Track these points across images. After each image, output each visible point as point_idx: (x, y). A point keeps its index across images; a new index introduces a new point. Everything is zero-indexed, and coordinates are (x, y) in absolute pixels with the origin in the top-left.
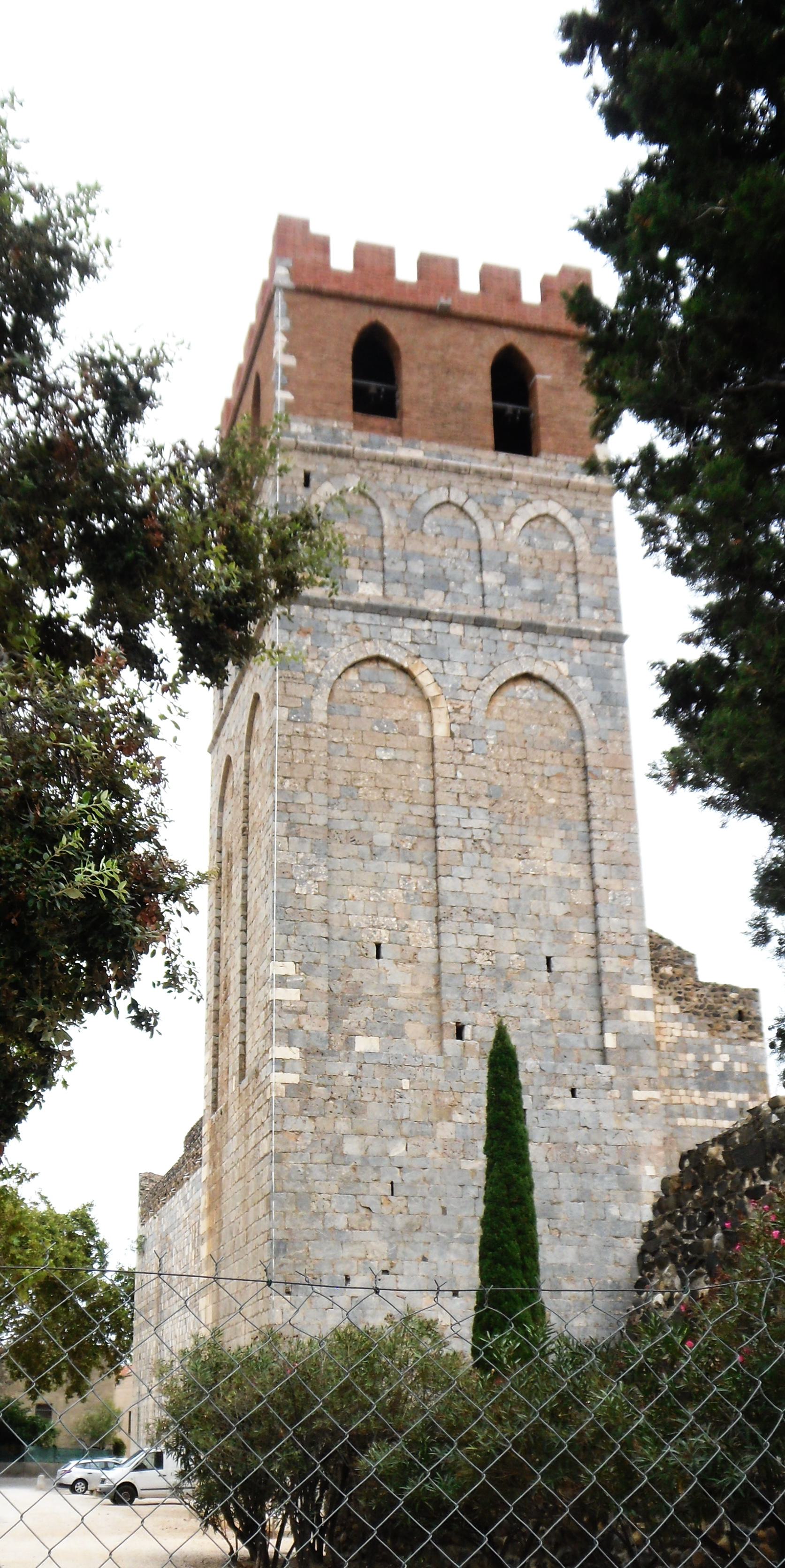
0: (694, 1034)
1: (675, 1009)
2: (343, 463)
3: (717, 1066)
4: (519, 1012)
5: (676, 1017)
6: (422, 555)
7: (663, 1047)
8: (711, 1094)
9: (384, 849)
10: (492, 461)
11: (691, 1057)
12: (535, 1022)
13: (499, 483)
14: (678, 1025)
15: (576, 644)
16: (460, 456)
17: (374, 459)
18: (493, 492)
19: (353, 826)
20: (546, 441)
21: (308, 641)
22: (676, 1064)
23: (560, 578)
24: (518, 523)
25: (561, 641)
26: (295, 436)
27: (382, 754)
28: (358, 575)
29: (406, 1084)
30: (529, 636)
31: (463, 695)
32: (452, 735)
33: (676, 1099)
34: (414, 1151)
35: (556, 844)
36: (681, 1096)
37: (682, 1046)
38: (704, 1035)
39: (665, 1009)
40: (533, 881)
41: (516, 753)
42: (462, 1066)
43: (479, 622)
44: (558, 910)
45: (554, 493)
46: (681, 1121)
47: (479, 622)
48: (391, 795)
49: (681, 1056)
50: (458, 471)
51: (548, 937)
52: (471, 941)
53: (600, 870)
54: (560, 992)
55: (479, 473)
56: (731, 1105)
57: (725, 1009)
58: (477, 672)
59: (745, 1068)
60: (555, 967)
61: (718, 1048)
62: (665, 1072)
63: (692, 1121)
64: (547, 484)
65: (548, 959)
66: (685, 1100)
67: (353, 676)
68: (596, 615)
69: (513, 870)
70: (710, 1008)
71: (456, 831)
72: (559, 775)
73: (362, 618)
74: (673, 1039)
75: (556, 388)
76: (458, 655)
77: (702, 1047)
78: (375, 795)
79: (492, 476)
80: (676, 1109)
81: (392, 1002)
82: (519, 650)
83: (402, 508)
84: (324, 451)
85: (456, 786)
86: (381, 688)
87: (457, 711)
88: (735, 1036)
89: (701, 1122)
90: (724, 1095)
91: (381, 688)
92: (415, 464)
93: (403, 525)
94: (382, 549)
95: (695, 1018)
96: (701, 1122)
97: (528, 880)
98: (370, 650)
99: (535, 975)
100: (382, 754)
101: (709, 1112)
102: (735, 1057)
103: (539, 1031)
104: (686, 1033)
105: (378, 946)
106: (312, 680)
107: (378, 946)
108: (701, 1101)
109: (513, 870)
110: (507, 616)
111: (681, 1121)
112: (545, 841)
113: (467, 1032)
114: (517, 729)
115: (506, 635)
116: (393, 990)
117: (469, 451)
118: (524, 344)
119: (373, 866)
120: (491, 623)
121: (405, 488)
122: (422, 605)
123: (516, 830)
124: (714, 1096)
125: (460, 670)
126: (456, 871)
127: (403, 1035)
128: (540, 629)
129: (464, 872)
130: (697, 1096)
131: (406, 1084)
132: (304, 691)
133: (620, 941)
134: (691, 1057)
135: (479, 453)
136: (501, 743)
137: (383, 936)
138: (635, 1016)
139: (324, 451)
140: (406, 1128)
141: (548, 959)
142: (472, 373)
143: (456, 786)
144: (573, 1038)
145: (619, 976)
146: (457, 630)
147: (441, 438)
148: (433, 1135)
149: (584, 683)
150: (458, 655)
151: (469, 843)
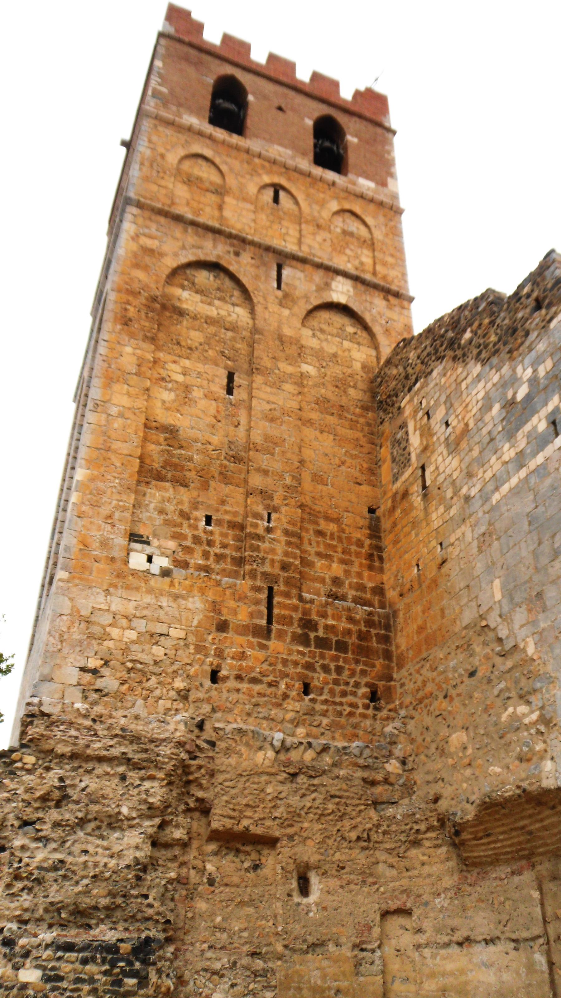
3: (522, 392)
5: (479, 378)
8: (520, 435)
22: (485, 431)
56: (542, 426)
57: (520, 315)
59: (549, 364)
62: (475, 453)
74: (480, 405)
88: (535, 334)
89: (514, 481)
102: (535, 364)
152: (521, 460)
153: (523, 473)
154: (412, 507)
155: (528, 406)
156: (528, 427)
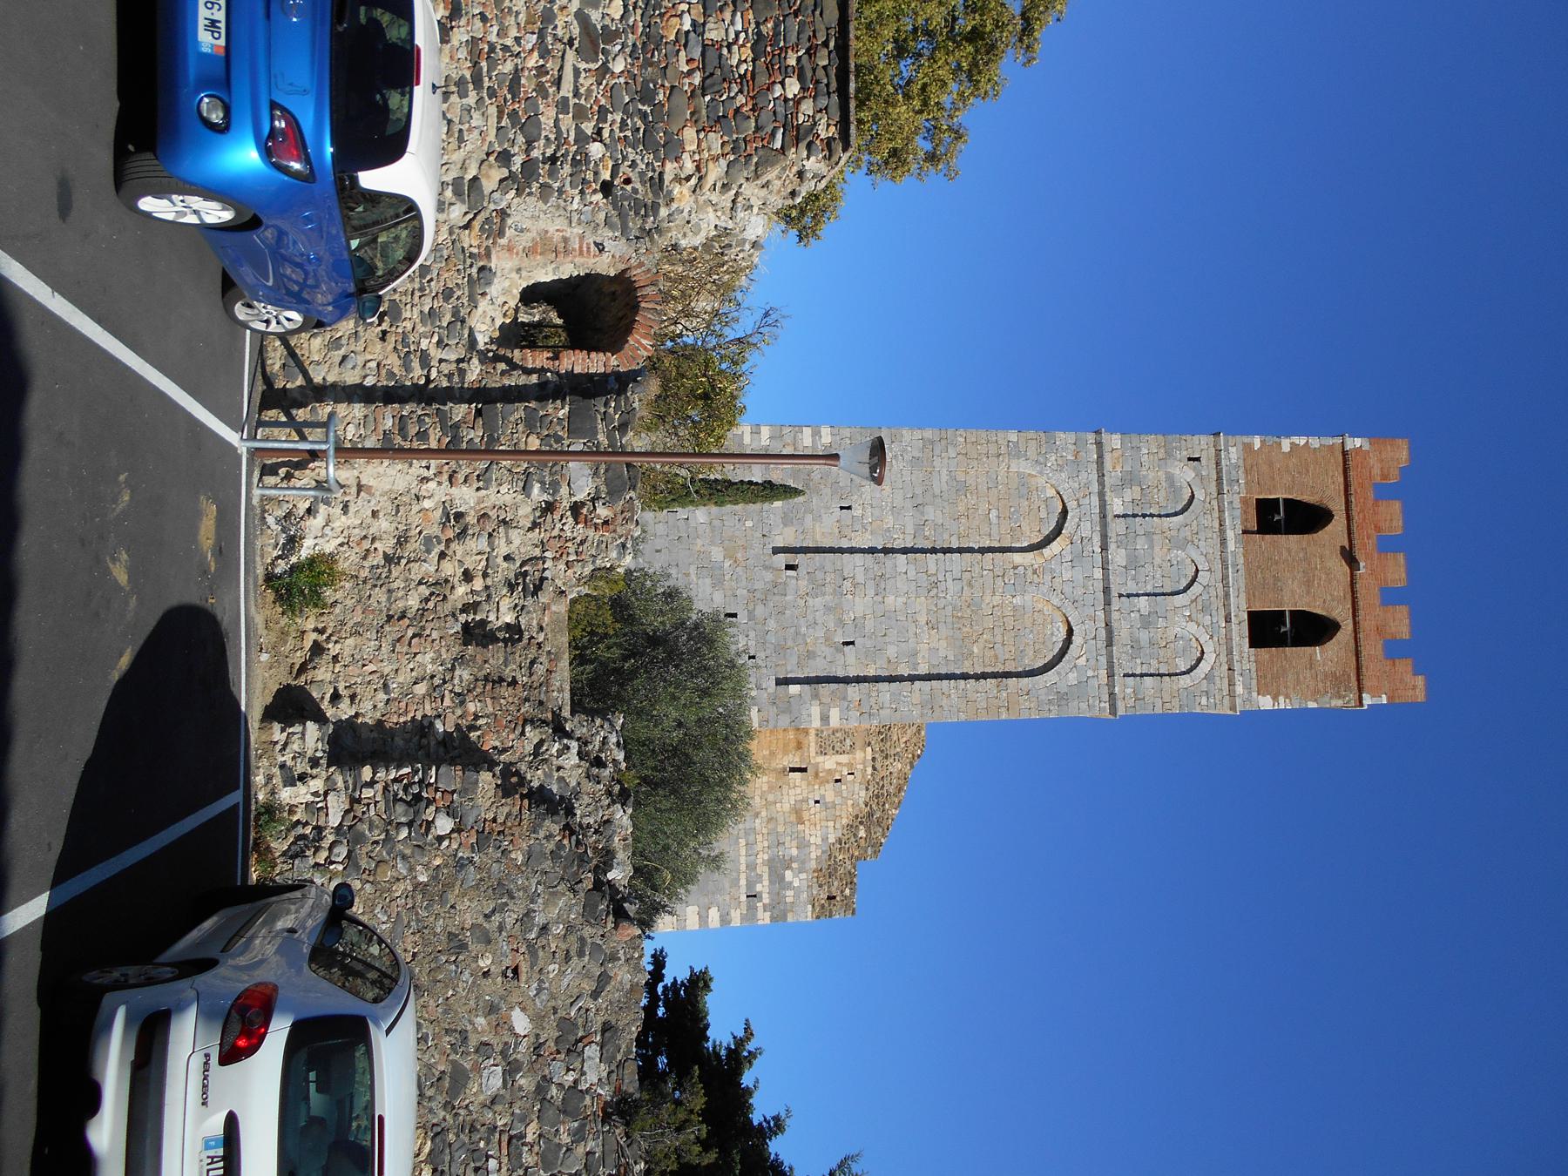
0: (813, 855)
1: (832, 840)
2: (1213, 488)
3: (788, 875)
4: (810, 617)
5: (825, 839)
6: (1152, 547)
7: (801, 827)
8: (766, 869)
9: (922, 513)
10: (1240, 609)
11: (794, 852)
12: (803, 630)
13: (1222, 613)
14: (819, 841)
15: (1103, 673)
16: (1237, 581)
17: (1221, 511)
18: (1214, 607)
19: (937, 492)
20: (1265, 653)
21: (1070, 457)
23: (1154, 662)
24: (1192, 627)
25: (1103, 660)
26: (1227, 450)
27: (994, 514)
28: (1128, 498)
29: (749, 524)
30: (1103, 633)
31: (1048, 577)
32: (1015, 568)
33: (759, 838)
34: (700, 529)
35: (942, 653)
36: (762, 843)
37: (803, 845)
38: (813, 865)
39: (831, 830)
40: (911, 634)
41: (1010, 622)
42: (766, 568)
43: (1106, 590)
44: (891, 651)
45: (1223, 658)
46: (742, 842)
47: (1106, 590)
48: (963, 520)
49: (794, 843)
50: (1225, 578)
51: (869, 644)
52: (860, 578)
53: (926, 685)
54: (828, 651)
55: (1227, 595)
56: (759, 888)
58: (1068, 589)
60: (847, 648)
61: (803, 876)
62: (780, 829)
63: (743, 852)
64: (1230, 652)
65: (852, 643)
66: (759, 847)
67: (1052, 493)
68: (1129, 691)
69: (918, 616)
70: (836, 870)
71: (942, 568)
72: (996, 657)
73: (1095, 500)
75: (1312, 663)
76: (1078, 574)
77: (803, 862)
78: (961, 508)
79: (1226, 606)
80: (751, 838)
81: (809, 517)
82: (1089, 625)
83: (1186, 532)
84: (1219, 472)
85: (977, 569)
86: (1043, 514)
87: (1035, 572)
89: (743, 860)
90: (766, 883)
91: (1043, 514)
92: (1223, 542)
93: (1174, 533)
94: (1152, 515)
95: (825, 856)
96: (743, 860)
97: (912, 629)
98: (1071, 505)
99: (840, 632)
100: (994, 514)
101: (751, 867)
102: (798, 891)
103: (797, 633)
104: (813, 848)
105: (849, 508)
106: (1041, 460)
107: (849, 508)
108: (759, 861)
109: (918, 616)
110: (1115, 616)
111: (742, 842)
112: (943, 643)
113: (790, 573)
114: (1028, 623)
115: (1101, 614)
116: (818, 518)
117: (1242, 585)
118: (1345, 635)
119: (909, 504)
120: (1108, 603)
121: (1202, 536)
122: (1112, 547)
123: (949, 620)
124: (764, 871)
125: (1067, 576)
126: (912, 567)
127: (785, 525)
128: (1110, 643)
129: (912, 574)
130: (763, 857)
131: (749, 524)
132: (1032, 453)
133: (873, 700)
134: (794, 852)
135: (1243, 596)
136: (1015, 609)
137: (857, 512)
138: (815, 711)
139: (1219, 472)
140: (716, 523)
141: (852, 643)
142: (1308, 593)
143: (977, 569)
144: (794, 660)
145: (844, 699)
146: (1098, 574)
147: (1247, 563)
148: (712, 543)
149: (1073, 678)
150: (1078, 574)
151: (934, 579)
152: (751, 867)
153: (743, 868)
154: (786, 753)
155: (777, 879)
156: (766, 876)
